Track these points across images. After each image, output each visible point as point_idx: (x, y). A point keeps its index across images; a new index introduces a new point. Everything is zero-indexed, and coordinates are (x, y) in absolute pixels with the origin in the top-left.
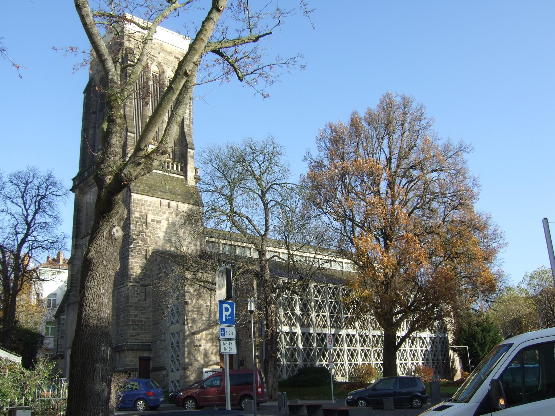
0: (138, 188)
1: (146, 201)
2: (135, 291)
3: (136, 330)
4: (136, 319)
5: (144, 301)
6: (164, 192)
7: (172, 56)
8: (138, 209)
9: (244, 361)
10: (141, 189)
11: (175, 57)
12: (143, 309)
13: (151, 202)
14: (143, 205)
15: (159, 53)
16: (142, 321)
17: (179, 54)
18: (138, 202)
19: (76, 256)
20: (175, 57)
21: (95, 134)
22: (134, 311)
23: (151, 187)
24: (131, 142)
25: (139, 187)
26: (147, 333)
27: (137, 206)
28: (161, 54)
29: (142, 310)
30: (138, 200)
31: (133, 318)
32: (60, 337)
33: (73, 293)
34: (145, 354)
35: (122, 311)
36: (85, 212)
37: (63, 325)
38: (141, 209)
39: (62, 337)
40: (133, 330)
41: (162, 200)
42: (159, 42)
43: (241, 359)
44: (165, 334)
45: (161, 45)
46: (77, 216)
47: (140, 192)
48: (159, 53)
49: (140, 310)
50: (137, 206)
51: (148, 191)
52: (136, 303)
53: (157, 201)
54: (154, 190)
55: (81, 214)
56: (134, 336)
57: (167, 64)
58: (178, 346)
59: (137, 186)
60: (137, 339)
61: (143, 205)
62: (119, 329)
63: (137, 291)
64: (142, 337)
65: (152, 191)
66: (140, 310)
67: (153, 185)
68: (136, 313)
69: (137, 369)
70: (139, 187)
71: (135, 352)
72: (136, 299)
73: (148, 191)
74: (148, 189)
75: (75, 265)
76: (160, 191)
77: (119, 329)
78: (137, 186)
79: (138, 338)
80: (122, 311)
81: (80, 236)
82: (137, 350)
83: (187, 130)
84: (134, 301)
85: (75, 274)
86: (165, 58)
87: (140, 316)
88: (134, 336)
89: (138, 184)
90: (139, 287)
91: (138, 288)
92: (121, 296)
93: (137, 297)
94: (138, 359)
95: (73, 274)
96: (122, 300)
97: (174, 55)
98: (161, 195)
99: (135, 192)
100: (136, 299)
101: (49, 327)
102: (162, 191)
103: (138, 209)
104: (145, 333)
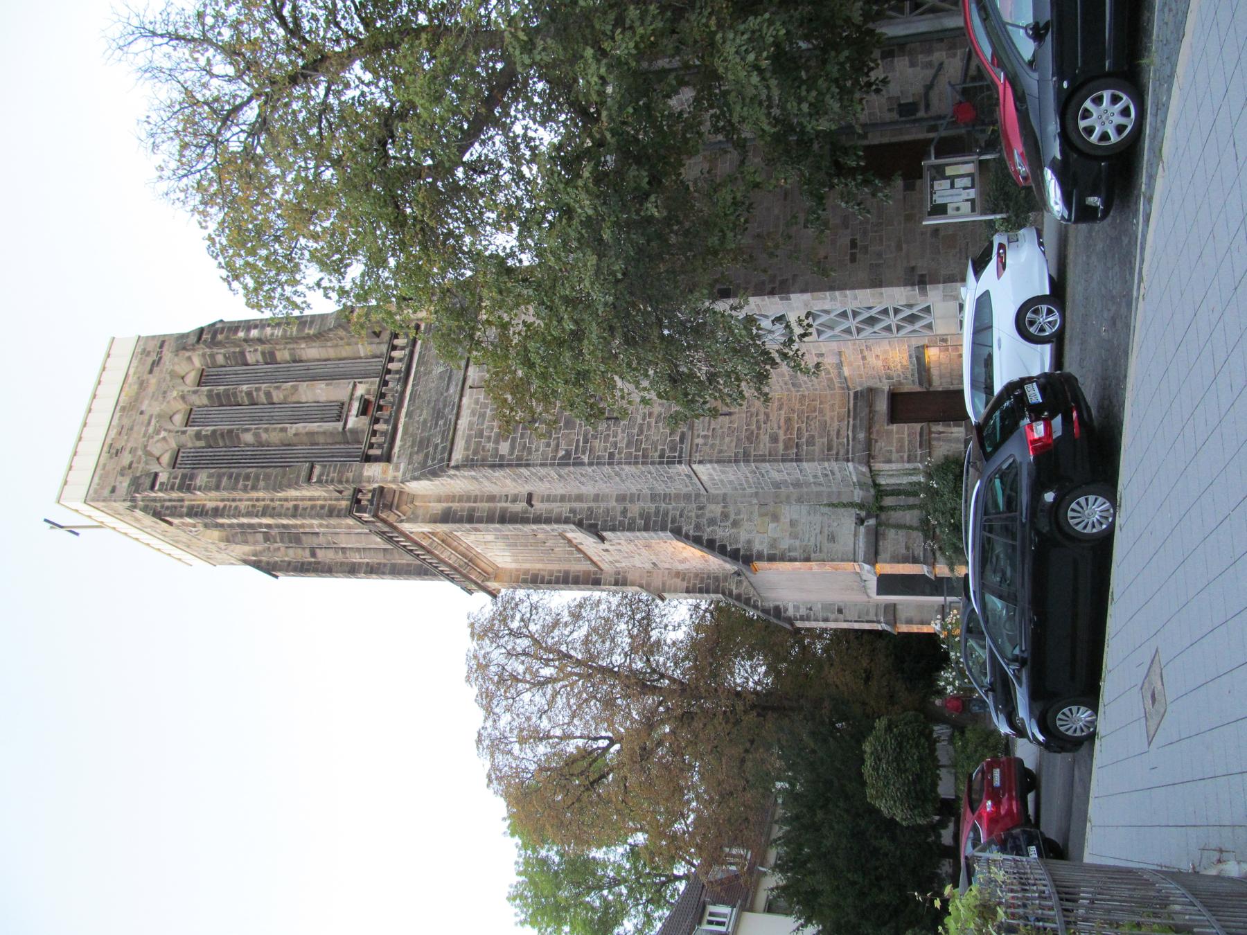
0: (440, 448)
1: (471, 424)
2: (705, 444)
3: (813, 437)
4: (782, 437)
5: (733, 417)
6: (450, 378)
7: (148, 380)
8: (490, 446)
9: (900, 105)
10: (442, 442)
11: (151, 372)
12: (755, 419)
13: (473, 413)
14: (480, 434)
15: (142, 413)
16: (788, 420)
17: (144, 364)
18: (473, 446)
19: (644, 582)
20: (151, 372)
21: (358, 550)
22: (762, 446)
23: (438, 414)
24: (334, 472)
25: (437, 445)
26: (821, 403)
27: (483, 450)
28: (144, 408)
29: (757, 421)
30: (467, 449)
31: (781, 446)
32: (841, 616)
33: (734, 588)
34: (882, 406)
35: (763, 476)
36: (539, 566)
37: (811, 609)
38: (489, 438)
39: (840, 611)
40: (814, 445)
41: (469, 383)
42: (118, 415)
43: (895, 116)
44: (822, 355)
45: (123, 409)
46: (549, 582)
47: (448, 444)
48: (142, 413)
49: (759, 428)
50: (483, 450)
51: (446, 420)
52: (739, 440)
53: (471, 396)
54: (445, 406)
55: (543, 573)
56: (830, 441)
57: (165, 392)
58: (855, 314)
59: (435, 453)
60: (838, 431)
61: (480, 434)
62: (812, 480)
63: (705, 437)
64: (832, 418)
65: (447, 411)
66: (759, 428)
67: (434, 409)
68: (765, 439)
69: (922, 428)
70: (437, 445)
71: (874, 436)
72: (727, 439)
73: (446, 420)
74: (441, 422)
75: (664, 584)
76: (447, 390)
77: (812, 480)
78: (435, 453)
79: (836, 428)
80: (763, 476)
81: (595, 573)
82: (869, 430)
83: (310, 328)
84: (734, 444)
85: (685, 584)
86: (153, 396)
87: (775, 426)
88: (830, 441)
89: (431, 449)
90: (696, 433)
91: (698, 436)
92: (722, 481)
93: (722, 438)
94: (894, 427)
95: (687, 588)
96: (733, 478)
97: (146, 376)
98: (457, 385)
99: (446, 455)
100: (727, 439)
101: (1121, 99)
102: (448, 385)
103: (490, 446)
104: (821, 411)
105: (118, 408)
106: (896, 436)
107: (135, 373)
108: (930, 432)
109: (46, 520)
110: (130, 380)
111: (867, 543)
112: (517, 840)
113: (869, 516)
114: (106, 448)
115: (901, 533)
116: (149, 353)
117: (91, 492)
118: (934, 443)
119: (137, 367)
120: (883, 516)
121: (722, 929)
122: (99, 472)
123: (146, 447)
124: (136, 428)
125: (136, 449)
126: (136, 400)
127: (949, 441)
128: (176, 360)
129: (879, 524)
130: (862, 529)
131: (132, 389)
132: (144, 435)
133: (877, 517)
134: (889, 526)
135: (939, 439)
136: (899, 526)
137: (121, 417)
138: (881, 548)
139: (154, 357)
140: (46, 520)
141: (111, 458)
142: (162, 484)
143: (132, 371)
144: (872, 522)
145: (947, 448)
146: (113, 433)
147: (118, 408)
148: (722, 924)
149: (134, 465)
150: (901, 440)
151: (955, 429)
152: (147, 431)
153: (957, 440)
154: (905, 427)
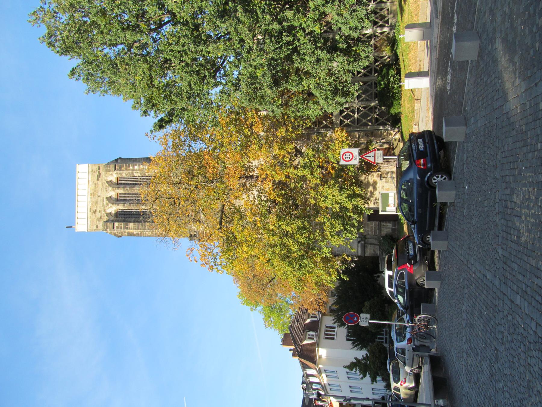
11: (98, 180)
15: (99, 196)
20: (98, 180)
28: (99, 195)
42: (90, 197)
45: (91, 195)
94: (370, 223)
105: (89, 194)
106: (370, 226)
107: (91, 180)
108: (381, 225)
109: (67, 227)
110: (90, 182)
111: (362, 249)
112: (239, 290)
113: (362, 240)
114: (89, 210)
115: (372, 246)
116: (95, 172)
117: (89, 227)
118: (382, 229)
119: (92, 177)
120: (366, 240)
121: (316, 319)
122: (89, 220)
123: (105, 210)
124: (99, 203)
125: (101, 211)
126: (95, 191)
127: (386, 228)
128: (107, 175)
129: (365, 243)
130: (360, 244)
131: (92, 187)
132: (103, 206)
133: (364, 241)
134: (368, 244)
135: (383, 227)
136: (371, 244)
137: (91, 198)
138: (366, 251)
139: (97, 174)
140: (67, 227)
141: (92, 214)
142: (117, 227)
143: (90, 179)
144: (363, 242)
145: (386, 230)
146: (90, 204)
147: (89, 194)
148: (316, 317)
149: (103, 217)
150: (372, 227)
151: (389, 224)
152: (103, 204)
153: (389, 228)
154: (373, 222)
